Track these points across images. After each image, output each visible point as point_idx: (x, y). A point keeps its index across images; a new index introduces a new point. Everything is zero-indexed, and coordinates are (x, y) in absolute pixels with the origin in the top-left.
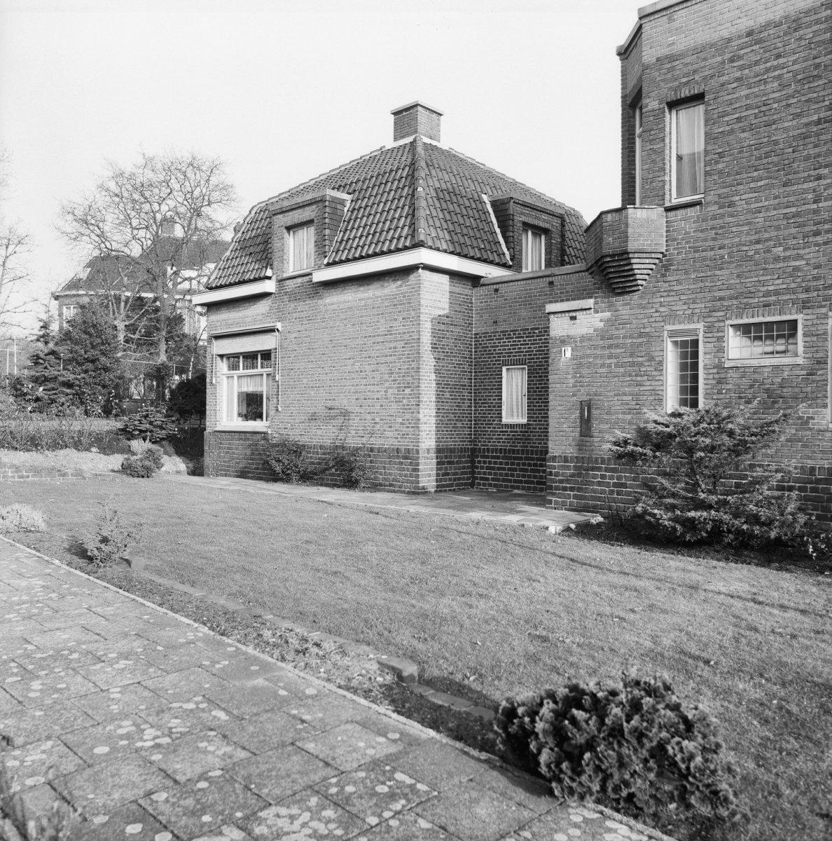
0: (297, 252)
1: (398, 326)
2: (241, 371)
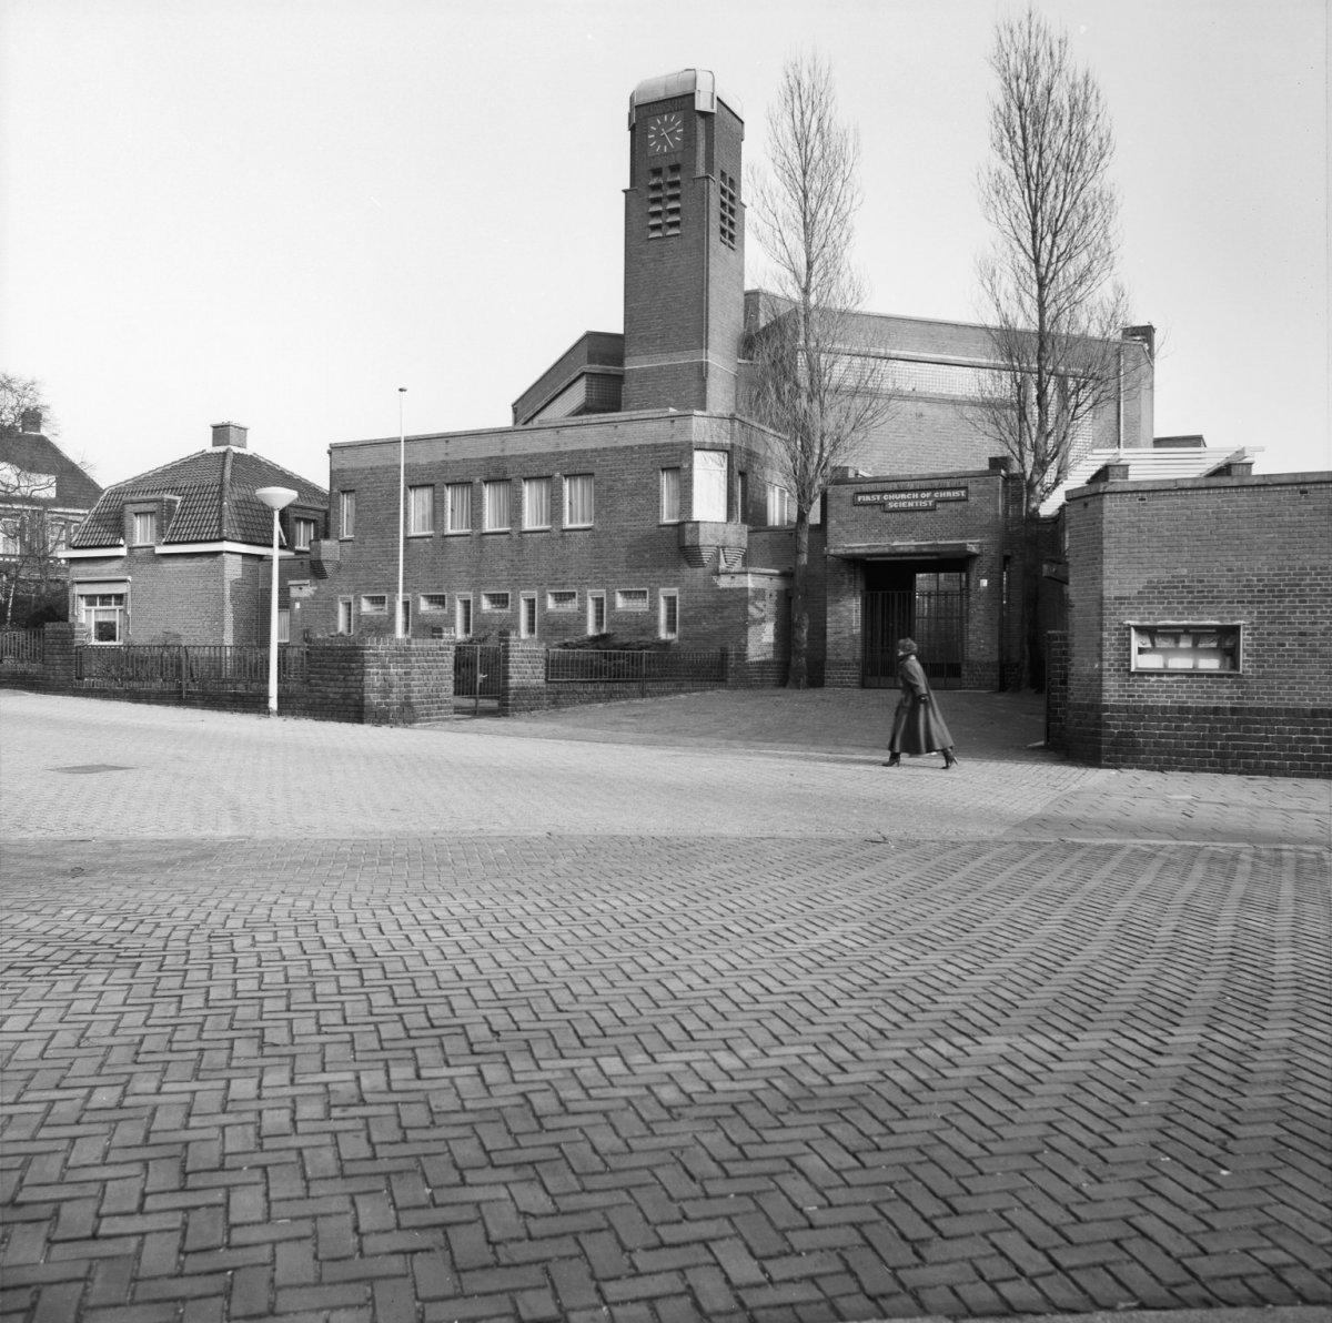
0: (142, 531)
1: (211, 585)
2: (98, 607)
